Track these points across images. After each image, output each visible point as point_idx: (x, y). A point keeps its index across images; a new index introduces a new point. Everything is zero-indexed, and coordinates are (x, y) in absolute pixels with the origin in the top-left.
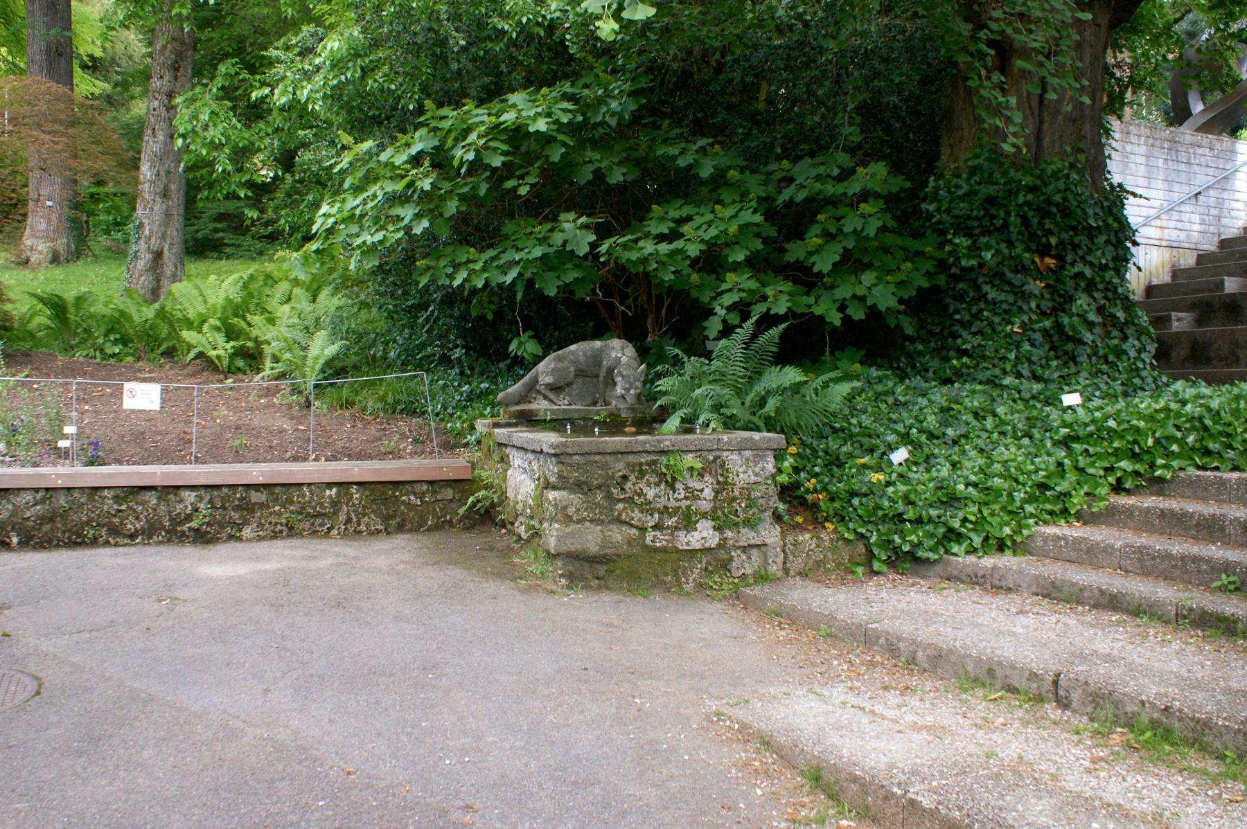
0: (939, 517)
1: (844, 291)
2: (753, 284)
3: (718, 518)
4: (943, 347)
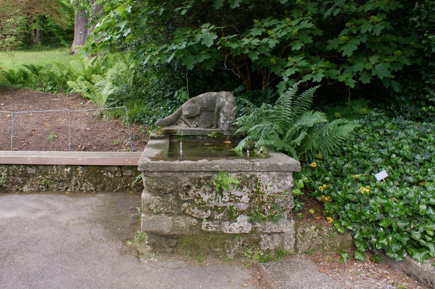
0: (405, 227)
1: (359, 67)
2: (304, 63)
3: (251, 215)
4: (417, 99)
